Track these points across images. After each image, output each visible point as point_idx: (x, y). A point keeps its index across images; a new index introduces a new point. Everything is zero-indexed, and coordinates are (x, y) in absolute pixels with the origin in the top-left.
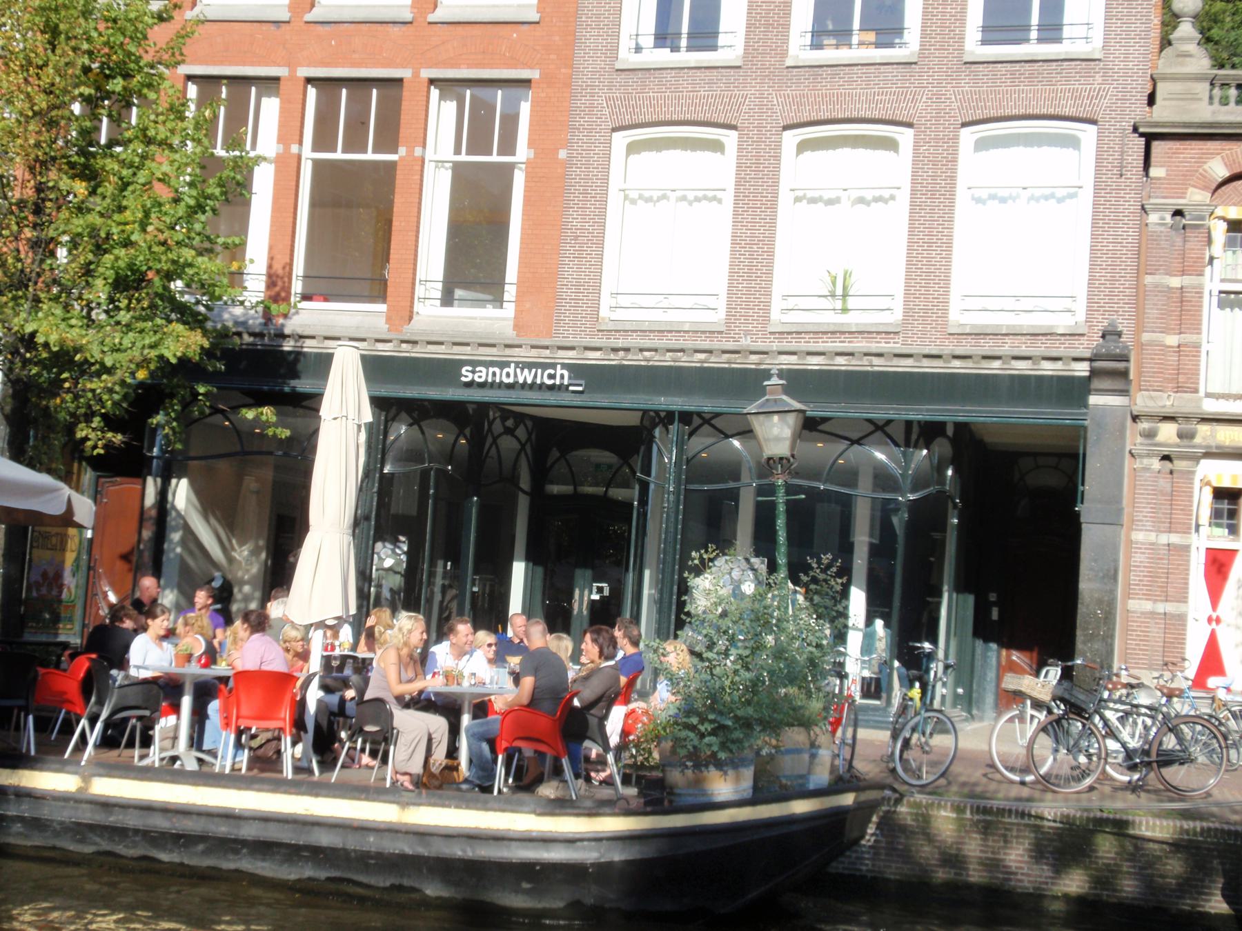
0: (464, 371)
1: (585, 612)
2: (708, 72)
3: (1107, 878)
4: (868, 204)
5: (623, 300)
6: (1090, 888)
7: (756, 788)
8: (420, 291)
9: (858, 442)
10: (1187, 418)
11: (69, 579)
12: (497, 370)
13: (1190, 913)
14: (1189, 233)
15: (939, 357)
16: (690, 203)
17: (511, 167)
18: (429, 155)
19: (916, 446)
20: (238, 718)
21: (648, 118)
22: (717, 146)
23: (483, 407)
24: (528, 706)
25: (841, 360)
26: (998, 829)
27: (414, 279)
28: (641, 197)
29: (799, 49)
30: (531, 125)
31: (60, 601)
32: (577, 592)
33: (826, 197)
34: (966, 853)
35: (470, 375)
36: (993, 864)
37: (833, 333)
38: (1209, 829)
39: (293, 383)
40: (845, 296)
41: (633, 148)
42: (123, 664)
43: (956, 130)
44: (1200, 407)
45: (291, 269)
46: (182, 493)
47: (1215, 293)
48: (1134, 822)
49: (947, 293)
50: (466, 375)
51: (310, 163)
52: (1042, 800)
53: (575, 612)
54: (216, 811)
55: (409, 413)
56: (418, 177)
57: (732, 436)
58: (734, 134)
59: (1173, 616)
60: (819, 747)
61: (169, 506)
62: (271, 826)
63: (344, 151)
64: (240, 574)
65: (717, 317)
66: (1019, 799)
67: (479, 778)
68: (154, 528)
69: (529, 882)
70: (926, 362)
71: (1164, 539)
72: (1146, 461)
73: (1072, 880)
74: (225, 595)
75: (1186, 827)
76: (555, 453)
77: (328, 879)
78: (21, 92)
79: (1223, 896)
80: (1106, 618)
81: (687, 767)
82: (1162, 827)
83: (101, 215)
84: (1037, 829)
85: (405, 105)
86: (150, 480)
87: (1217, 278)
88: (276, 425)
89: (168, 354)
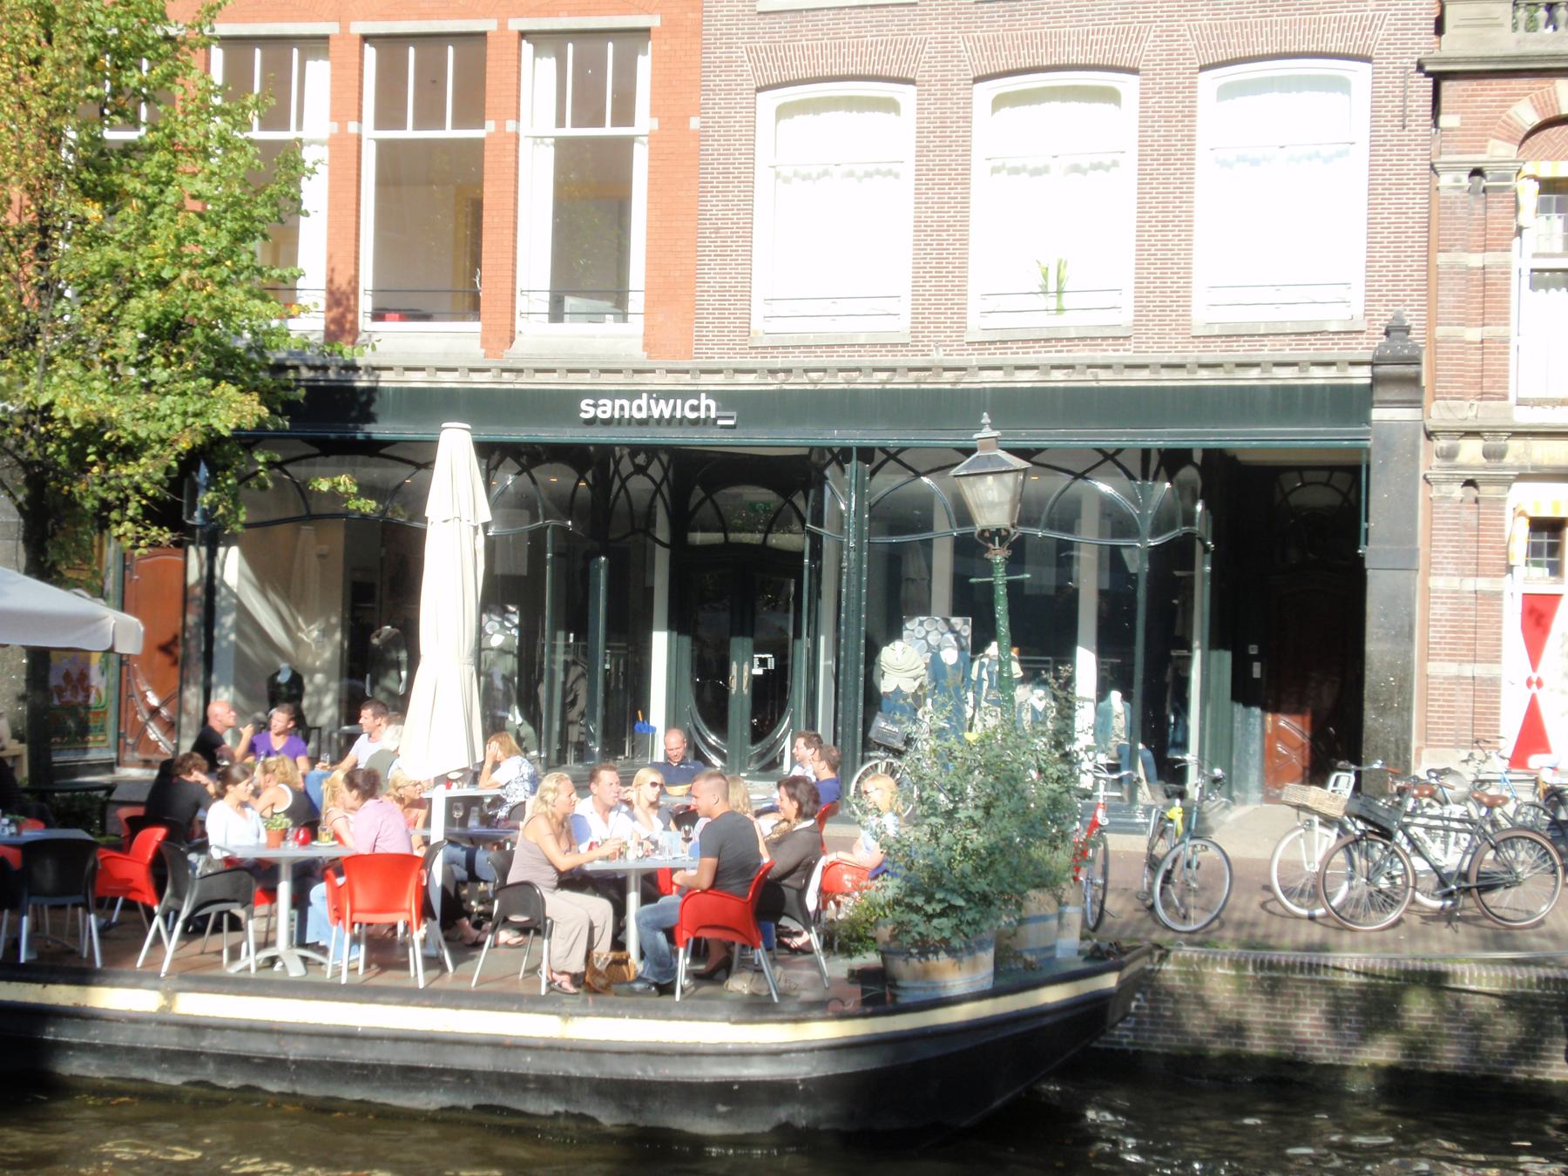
0: (583, 405)
1: (746, 691)
3: (1424, 1042)
4: (1085, 172)
5: (778, 307)
6: (1404, 1056)
7: (997, 973)
8: (521, 304)
9: (1081, 476)
10: (1495, 433)
12: (626, 403)
13: (1527, 1082)
14: (1491, 197)
16: (860, 180)
17: (628, 142)
18: (525, 129)
19: (1155, 479)
20: (352, 911)
21: (802, 74)
22: (890, 106)
23: (606, 450)
24: (712, 887)
25: (1058, 375)
26: (1287, 987)
27: (514, 289)
30: (653, 87)
31: (88, 707)
32: (734, 667)
33: (1030, 167)
34: (1249, 1018)
36: (1279, 1033)
38: (1547, 979)
40: (1059, 292)
41: (784, 111)
42: (203, 847)
43: (1192, 76)
45: (357, 283)
46: (232, 565)
48: (1455, 973)
49: (1188, 285)
50: (587, 410)
52: (1339, 948)
53: (733, 691)
54: (334, 1030)
55: (517, 460)
56: (512, 159)
57: (925, 474)
58: (910, 90)
59: (1483, 681)
60: (1067, 904)
61: (216, 582)
62: (403, 1046)
63: (417, 127)
64: (309, 660)
65: (900, 326)
66: (1309, 948)
67: (655, 975)
68: (201, 611)
69: (724, 1104)
70: (1165, 374)
71: (1470, 584)
72: (1444, 488)
73: (1380, 1046)
74: (294, 691)
75: (1519, 977)
76: (698, 493)
77: (478, 1107)
78: (12, 93)
80: (1401, 686)
81: (911, 955)
82: (1489, 978)
83: (125, 247)
84: (1331, 986)
85: (491, 66)
86: (192, 550)
87: (1527, 253)
88: (357, 496)
89: (217, 425)
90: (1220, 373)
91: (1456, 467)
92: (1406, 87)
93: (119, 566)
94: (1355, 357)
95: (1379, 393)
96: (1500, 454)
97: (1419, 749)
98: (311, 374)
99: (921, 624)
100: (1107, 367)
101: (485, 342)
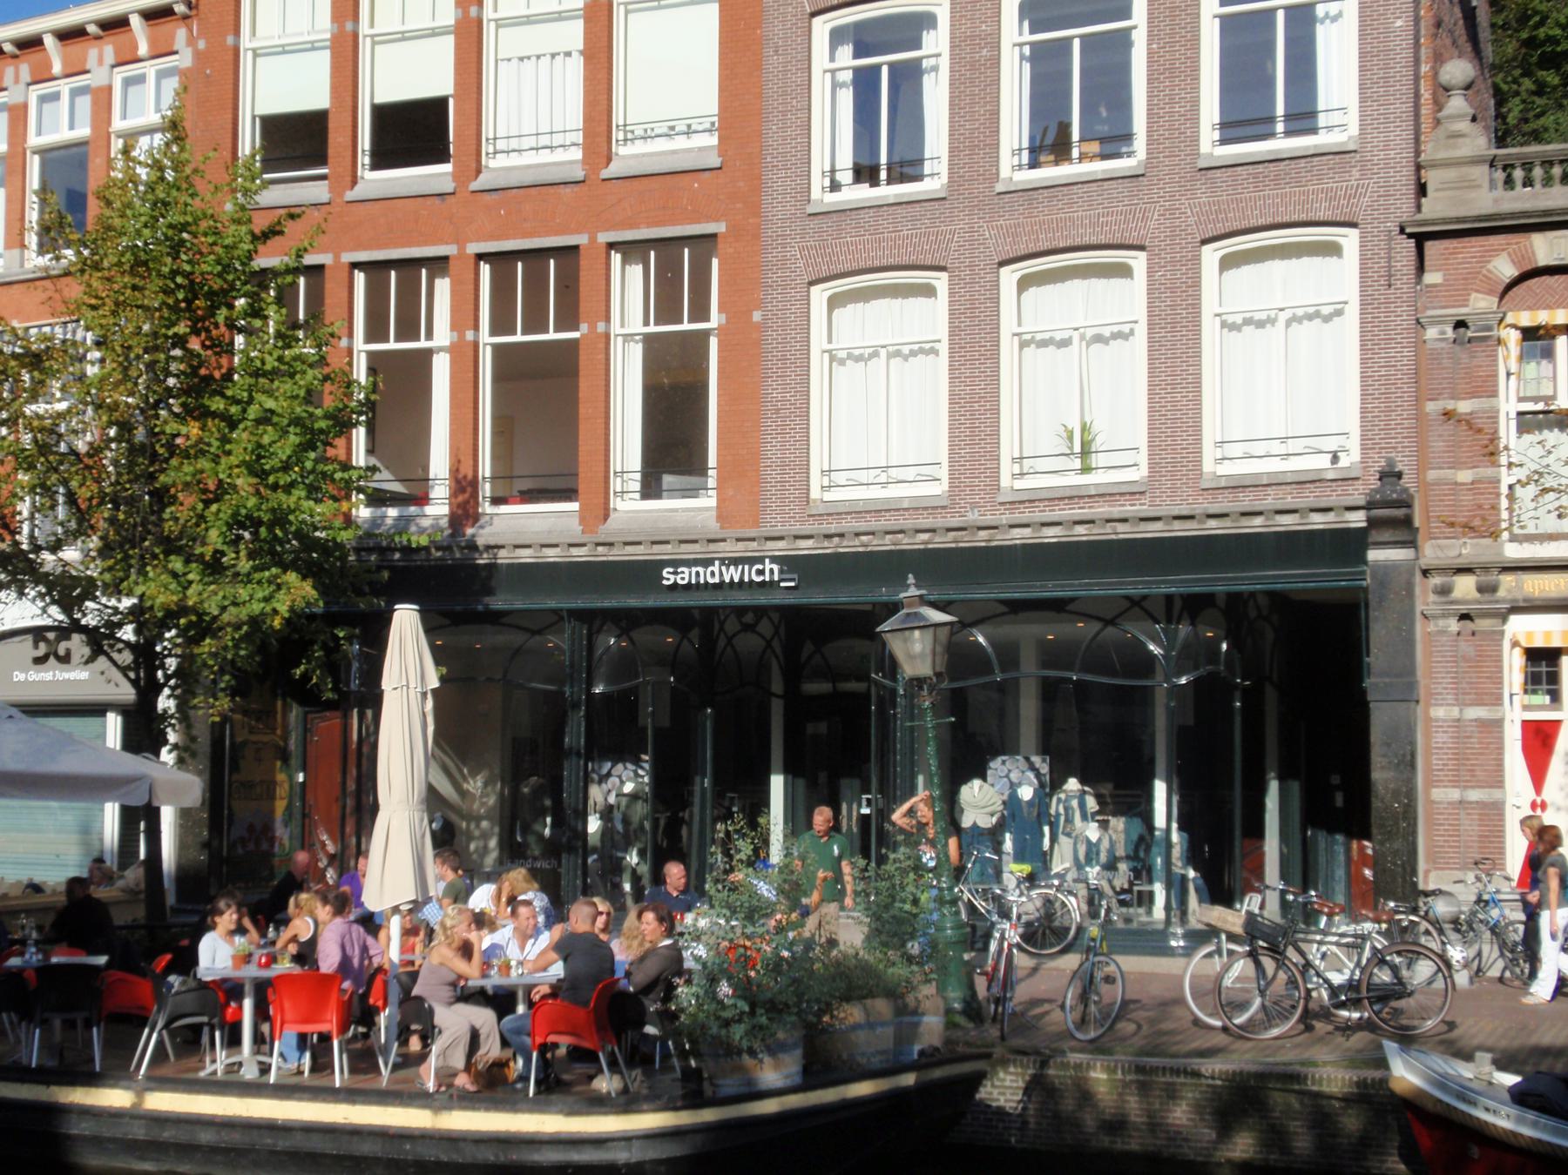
0: (665, 574)
2: (909, 208)
5: (1236, 450)
7: (806, 1070)
8: (616, 484)
10: (1486, 569)
11: (281, 832)
12: (701, 570)
15: (1191, 517)
16: (906, 358)
18: (616, 328)
25: (1080, 529)
28: (850, 356)
29: (1012, 169)
35: (672, 577)
36: (1155, 1125)
37: (1070, 498)
39: (487, 600)
44: (1501, 553)
47: (1513, 415)
51: (489, 349)
56: (602, 356)
60: (923, 1014)
70: (1177, 525)
72: (1441, 623)
76: (808, 648)
79: (1401, 1155)
90: (1227, 522)
91: (1452, 603)
92: (1390, 249)
93: (300, 729)
94: (1350, 501)
95: (1375, 536)
96: (1493, 589)
97: (1427, 872)
98: (439, 554)
99: (1004, 762)
100: (1125, 520)
101: (582, 520)
